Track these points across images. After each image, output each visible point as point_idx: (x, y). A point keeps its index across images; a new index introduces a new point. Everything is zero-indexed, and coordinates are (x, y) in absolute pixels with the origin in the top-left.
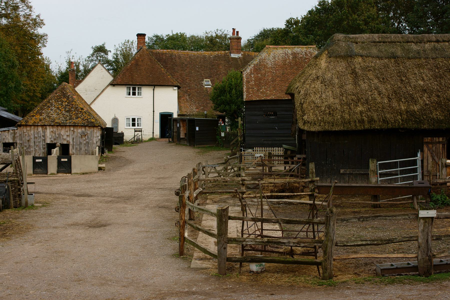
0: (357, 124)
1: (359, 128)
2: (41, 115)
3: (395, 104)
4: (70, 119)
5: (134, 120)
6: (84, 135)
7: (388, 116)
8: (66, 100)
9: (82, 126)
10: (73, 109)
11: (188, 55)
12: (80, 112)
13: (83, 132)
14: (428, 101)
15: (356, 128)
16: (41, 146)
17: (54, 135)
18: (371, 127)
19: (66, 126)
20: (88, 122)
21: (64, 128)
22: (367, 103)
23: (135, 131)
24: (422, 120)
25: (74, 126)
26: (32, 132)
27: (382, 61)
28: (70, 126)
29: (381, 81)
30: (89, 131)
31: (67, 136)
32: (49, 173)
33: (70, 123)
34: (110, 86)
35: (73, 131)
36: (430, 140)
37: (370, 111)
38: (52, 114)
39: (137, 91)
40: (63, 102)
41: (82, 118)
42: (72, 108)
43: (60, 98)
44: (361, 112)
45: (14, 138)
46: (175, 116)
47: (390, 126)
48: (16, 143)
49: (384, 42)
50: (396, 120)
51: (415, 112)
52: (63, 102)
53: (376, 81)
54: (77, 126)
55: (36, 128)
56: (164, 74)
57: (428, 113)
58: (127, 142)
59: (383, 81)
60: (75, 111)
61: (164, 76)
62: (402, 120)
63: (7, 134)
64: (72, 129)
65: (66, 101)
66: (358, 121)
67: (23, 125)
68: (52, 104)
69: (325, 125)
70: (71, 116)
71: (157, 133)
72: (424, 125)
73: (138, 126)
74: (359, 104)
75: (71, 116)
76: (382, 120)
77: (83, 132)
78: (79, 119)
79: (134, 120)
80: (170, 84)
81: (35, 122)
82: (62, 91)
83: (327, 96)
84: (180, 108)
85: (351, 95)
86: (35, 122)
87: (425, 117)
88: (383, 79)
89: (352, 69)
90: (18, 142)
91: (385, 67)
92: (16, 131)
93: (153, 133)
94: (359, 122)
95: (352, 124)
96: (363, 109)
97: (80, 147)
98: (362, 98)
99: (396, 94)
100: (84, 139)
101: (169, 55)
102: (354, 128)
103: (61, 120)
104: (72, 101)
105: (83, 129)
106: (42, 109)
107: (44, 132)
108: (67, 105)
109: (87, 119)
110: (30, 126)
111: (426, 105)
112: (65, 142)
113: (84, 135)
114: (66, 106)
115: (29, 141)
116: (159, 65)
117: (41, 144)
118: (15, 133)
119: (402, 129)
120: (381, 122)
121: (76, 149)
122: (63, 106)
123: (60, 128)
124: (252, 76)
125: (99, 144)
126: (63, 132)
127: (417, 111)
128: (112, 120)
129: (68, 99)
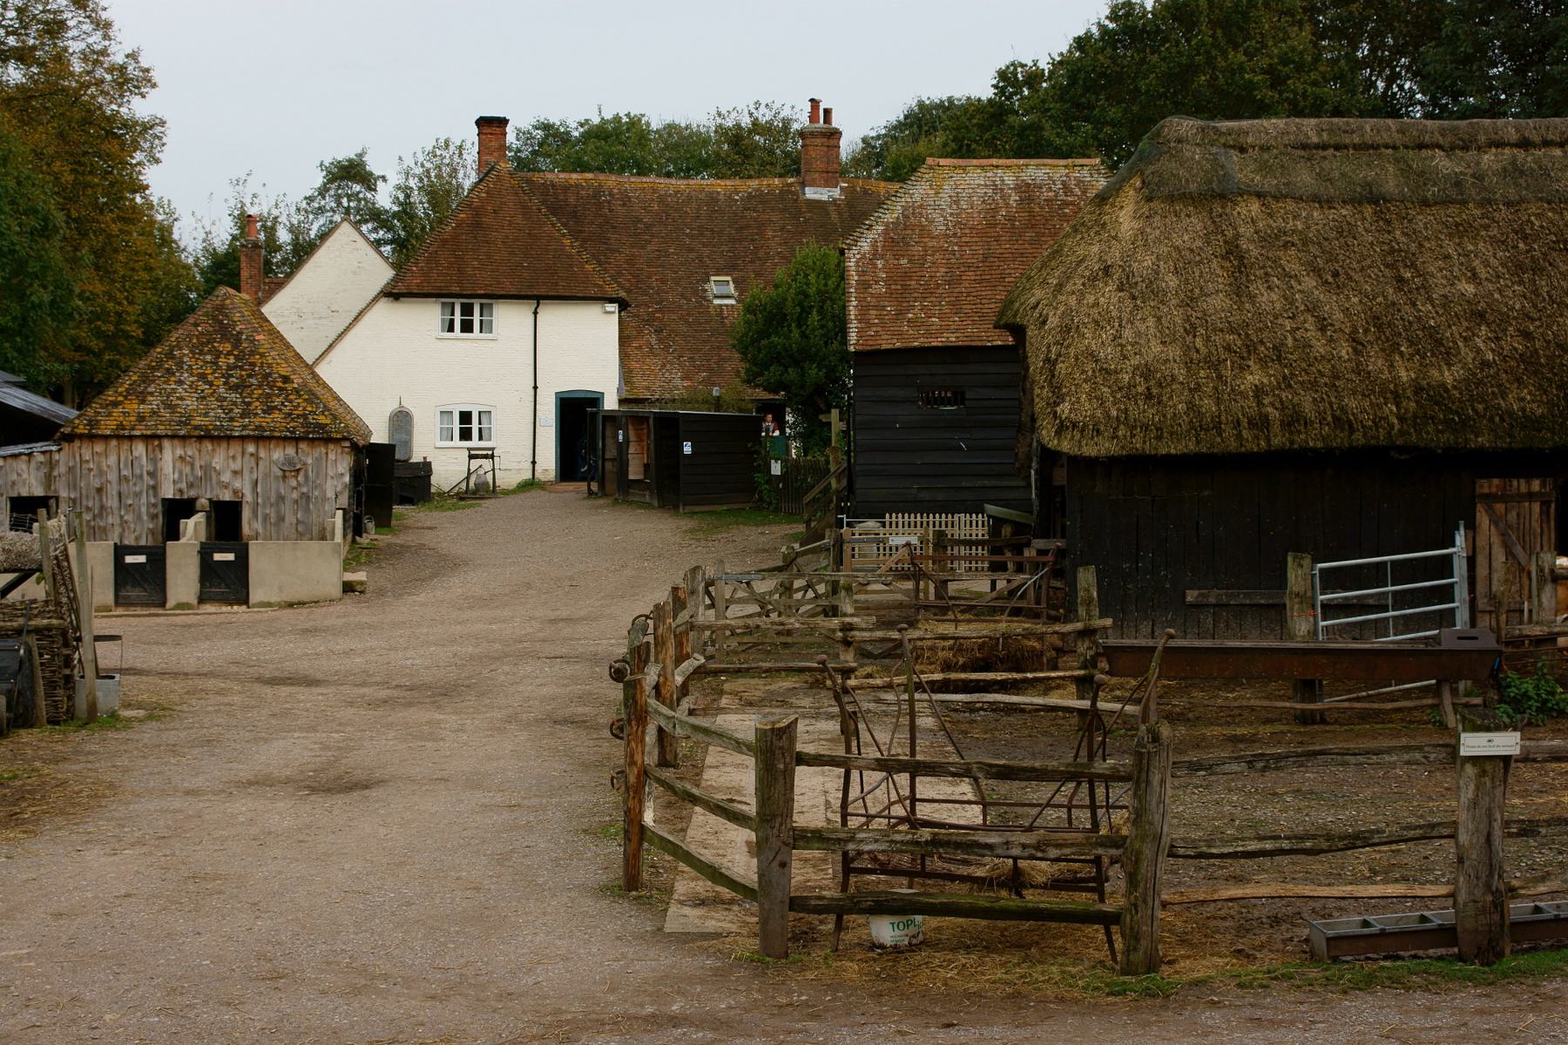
0: (1245, 433)
1: (1252, 447)
2: (143, 402)
3: (1375, 363)
4: (243, 416)
5: (465, 417)
6: (291, 470)
7: (1352, 403)
8: (228, 347)
9: (285, 439)
10: (253, 381)
11: (655, 191)
12: (280, 389)
13: (290, 462)
14: (1493, 350)
15: (1242, 445)
16: (144, 509)
17: (187, 470)
18: (1292, 443)
19: (229, 438)
20: (306, 425)
21: (224, 445)
22: (1279, 358)
23: (471, 457)
24: (1469, 418)
25: (259, 439)
26: (112, 460)
27: (1332, 214)
28: (243, 438)
29: (1326, 282)
30: (309, 455)
31: (235, 473)
32: (171, 603)
33: (244, 427)
34: (384, 300)
35: (256, 456)
36: (1497, 487)
37: (1290, 386)
38: (181, 399)
39: (476, 318)
40: (218, 354)
41: (286, 410)
42: (250, 376)
43: (209, 342)
44: (1259, 392)
45: (49, 480)
46: (611, 403)
47: (1358, 438)
48: (57, 498)
49: (1337, 147)
50: (1381, 418)
51: (1447, 390)
52: (218, 354)
53: (1310, 282)
54: (270, 438)
55: (126, 446)
56: (570, 256)
57: (1493, 393)
58: (441, 494)
59: (1336, 282)
60: (260, 386)
61: (571, 266)
62: (1401, 419)
63: (24, 466)
64: (251, 448)
65: (229, 353)
66: (1249, 423)
67: (81, 437)
68: (180, 364)
69: (1133, 436)
70: (249, 404)
71: (548, 462)
72: (1477, 436)
73: (481, 438)
74: (1251, 363)
75: (249, 404)
76: (1329, 419)
77: (290, 462)
78: (277, 415)
79: (465, 417)
80: (592, 292)
81: (121, 426)
82: (214, 318)
83: (1138, 334)
84: (626, 374)
85: (1221, 330)
86: (121, 426)
87: (1480, 407)
88: (1336, 275)
89: (1225, 242)
90: (63, 494)
91: (1341, 233)
92: (56, 457)
93: (534, 463)
94: (1252, 424)
95: (1228, 431)
96: (1265, 381)
97: (278, 512)
98: (1262, 342)
99: (1379, 327)
100: (294, 483)
101: (590, 192)
102: (1233, 445)
103: (212, 417)
104: (252, 353)
105: (290, 451)
106: (146, 380)
107: (154, 461)
108: (236, 367)
109: (305, 416)
110: (106, 438)
111: (1485, 364)
112: (227, 496)
113: (291, 470)
114: (230, 368)
115: (99, 490)
116: (553, 225)
117: (144, 500)
118: (52, 465)
119: (1401, 449)
120: (1328, 424)
121: (266, 517)
122: (219, 368)
123: (208, 445)
124: (880, 263)
125: (344, 500)
126: (221, 459)
127: (1455, 387)
128: (391, 419)
129: (235, 347)
